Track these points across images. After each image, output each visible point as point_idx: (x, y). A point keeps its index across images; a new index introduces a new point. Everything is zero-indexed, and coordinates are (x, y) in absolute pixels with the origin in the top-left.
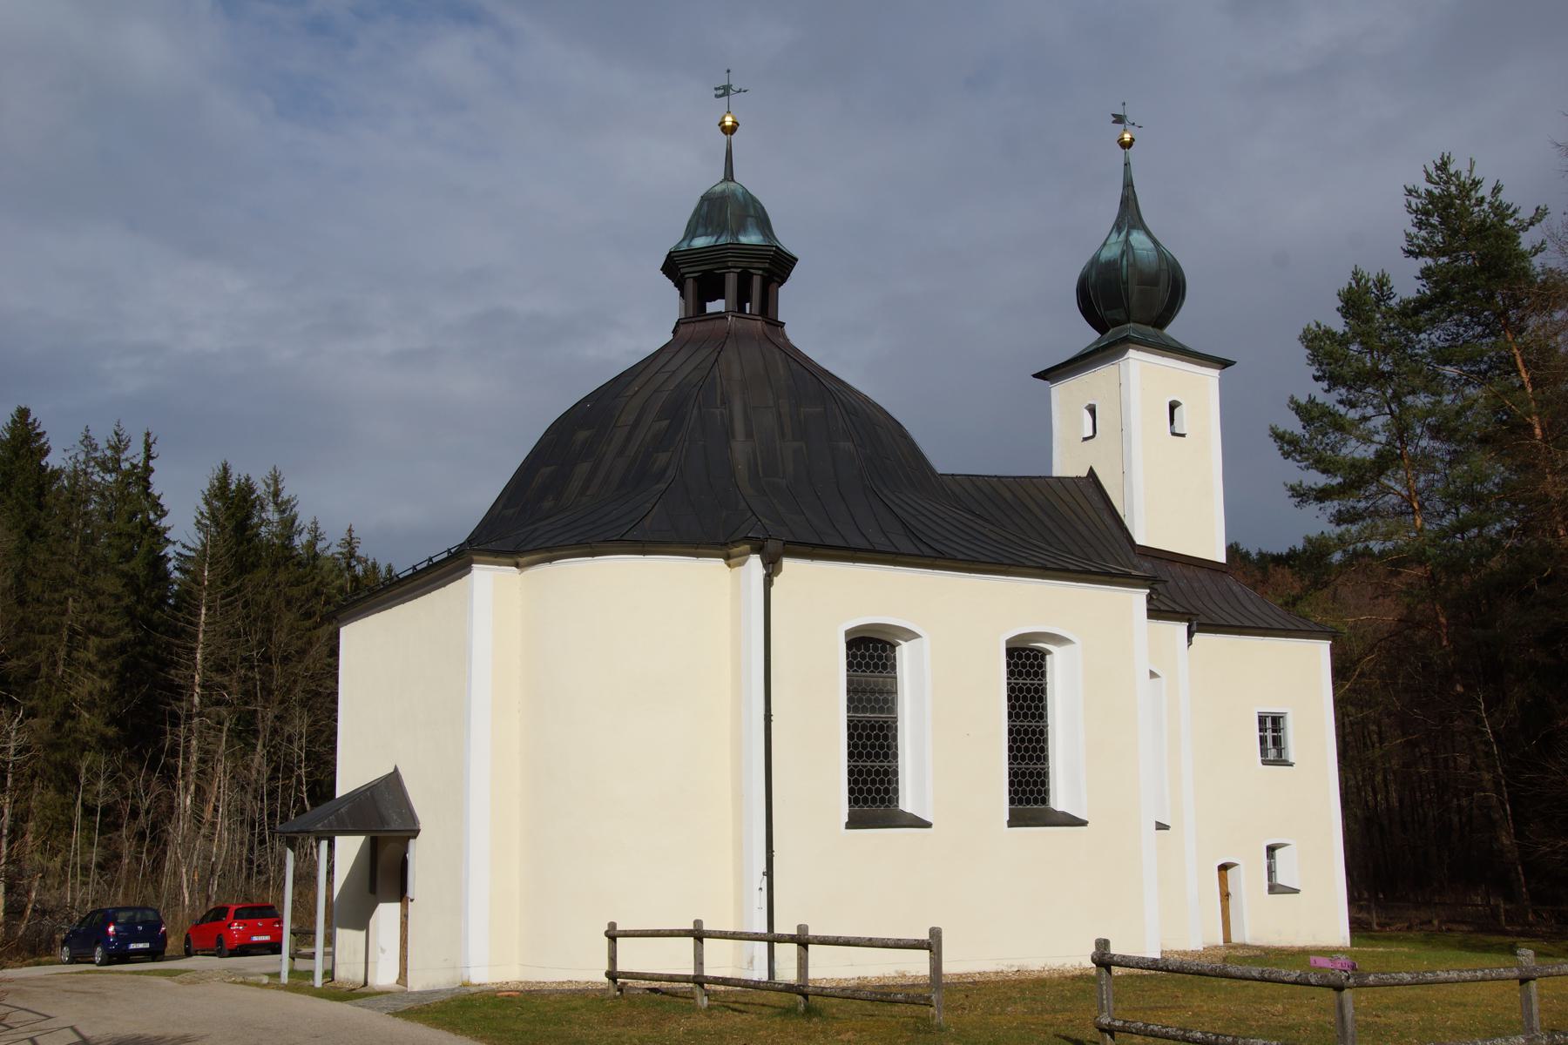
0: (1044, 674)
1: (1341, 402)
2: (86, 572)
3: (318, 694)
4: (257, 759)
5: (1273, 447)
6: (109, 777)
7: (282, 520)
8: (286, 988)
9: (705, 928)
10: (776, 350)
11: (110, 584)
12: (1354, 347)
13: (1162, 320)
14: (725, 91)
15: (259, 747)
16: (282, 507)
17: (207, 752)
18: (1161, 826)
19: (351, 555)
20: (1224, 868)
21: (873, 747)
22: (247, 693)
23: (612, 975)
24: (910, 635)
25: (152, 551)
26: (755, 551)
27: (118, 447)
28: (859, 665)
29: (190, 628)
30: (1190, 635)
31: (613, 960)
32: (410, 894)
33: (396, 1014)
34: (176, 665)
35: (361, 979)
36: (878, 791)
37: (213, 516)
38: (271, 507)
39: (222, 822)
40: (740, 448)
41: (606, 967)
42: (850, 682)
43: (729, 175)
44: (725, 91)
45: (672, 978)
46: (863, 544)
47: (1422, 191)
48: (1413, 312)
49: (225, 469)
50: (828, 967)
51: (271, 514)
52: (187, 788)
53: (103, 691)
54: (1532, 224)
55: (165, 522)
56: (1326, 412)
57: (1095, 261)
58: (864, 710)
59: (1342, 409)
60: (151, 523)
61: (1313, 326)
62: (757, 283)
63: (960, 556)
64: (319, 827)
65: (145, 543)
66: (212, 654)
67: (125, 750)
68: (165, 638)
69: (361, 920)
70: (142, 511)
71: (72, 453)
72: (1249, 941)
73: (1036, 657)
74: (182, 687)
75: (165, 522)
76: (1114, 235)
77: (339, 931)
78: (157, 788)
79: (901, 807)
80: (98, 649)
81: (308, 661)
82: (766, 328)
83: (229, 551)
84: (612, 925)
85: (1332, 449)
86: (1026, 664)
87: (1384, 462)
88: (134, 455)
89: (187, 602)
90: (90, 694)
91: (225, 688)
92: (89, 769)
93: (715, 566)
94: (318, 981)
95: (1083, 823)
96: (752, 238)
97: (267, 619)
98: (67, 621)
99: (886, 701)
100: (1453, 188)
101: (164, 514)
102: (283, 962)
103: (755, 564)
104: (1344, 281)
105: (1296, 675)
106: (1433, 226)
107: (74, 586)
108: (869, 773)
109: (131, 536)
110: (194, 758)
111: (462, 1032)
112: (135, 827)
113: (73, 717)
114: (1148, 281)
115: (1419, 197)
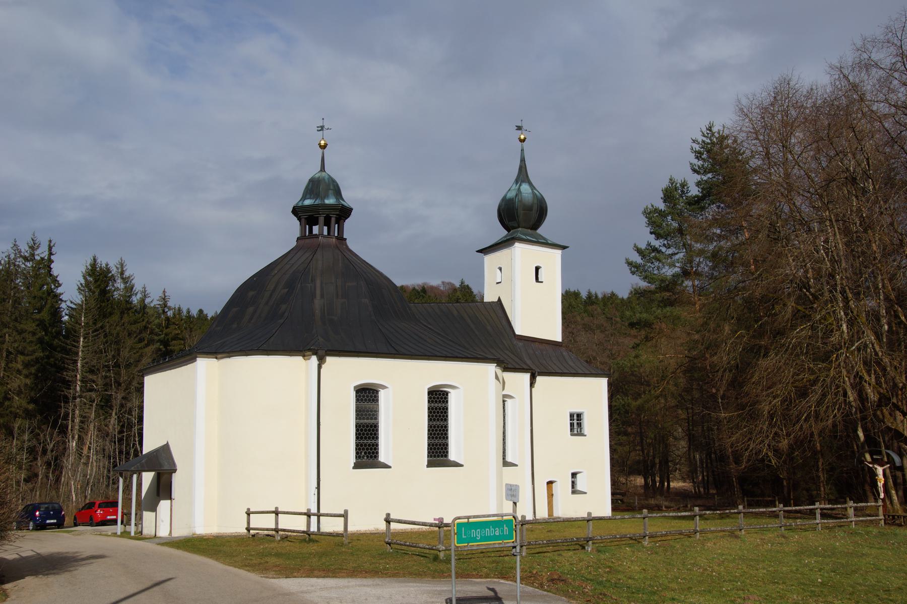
1: (664, 245)
2: (16, 320)
4: (113, 420)
6: (32, 432)
8: (119, 536)
11: (30, 326)
12: (669, 218)
13: (536, 225)
15: (114, 414)
16: (126, 280)
17: (85, 417)
19: (165, 306)
20: (550, 483)
23: (248, 529)
24: (384, 387)
25: (52, 306)
26: (314, 354)
31: (249, 523)
34: (67, 369)
38: (119, 281)
39: (93, 458)
40: (318, 303)
42: (357, 408)
44: (322, 128)
47: (700, 140)
48: (697, 203)
49: (95, 260)
51: (120, 284)
52: (73, 438)
53: (26, 385)
55: (60, 290)
56: (655, 250)
57: (505, 196)
58: (364, 419)
59: (663, 249)
61: (650, 206)
62: (333, 220)
64: (133, 468)
66: (86, 363)
67: (39, 417)
69: (153, 508)
70: (47, 284)
71: (6, 254)
75: (60, 290)
77: (145, 513)
78: (57, 438)
84: (249, 509)
86: (438, 400)
89: (72, 334)
90: (19, 386)
91: (94, 382)
92: (19, 428)
93: (299, 359)
96: (330, 201)
97: (117, 343)
98: (5, 346)
101: (60, 285)
102: (119, 528)
103: (314, 360)
104: (665, 184)
107: (9, 328)
108: (365, 445)
110: (77, 420)
112: (45, 459)
113: (9, 399)
114: (528, 208)
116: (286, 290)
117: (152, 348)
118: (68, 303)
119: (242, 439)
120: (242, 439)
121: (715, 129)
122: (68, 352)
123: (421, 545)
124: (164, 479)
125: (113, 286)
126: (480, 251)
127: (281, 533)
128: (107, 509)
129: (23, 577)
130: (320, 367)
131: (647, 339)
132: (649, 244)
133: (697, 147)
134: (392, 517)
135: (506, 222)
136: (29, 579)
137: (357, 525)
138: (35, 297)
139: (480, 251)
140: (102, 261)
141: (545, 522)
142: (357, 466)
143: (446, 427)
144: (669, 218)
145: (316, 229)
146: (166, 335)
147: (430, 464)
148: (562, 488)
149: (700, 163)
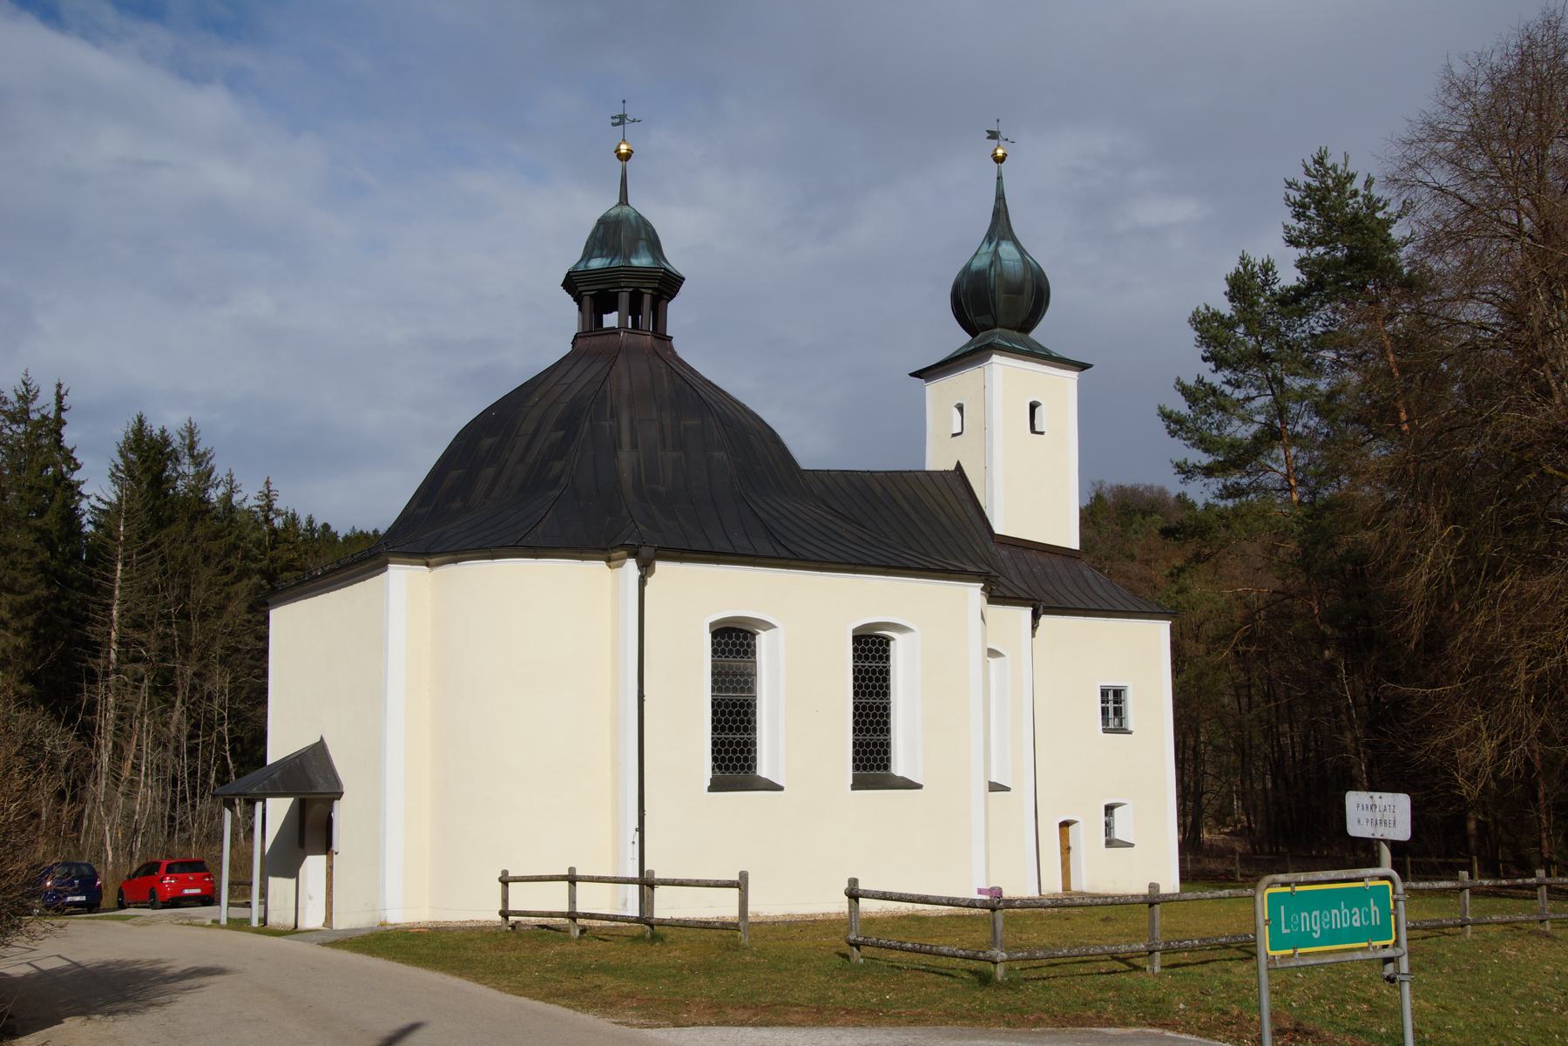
0: (888, 658)
1: (1229, 382)
3: (238, 650)
4: (176, 715)
5: (1161, 425)
7: (198, 475)
8: (222, 927)
9: (578, 873)
10: (662, 364)
12: (1241, 330)
14: (621, 120)
15: (178, 704)
16: (198, 460)
17: (125, 709)
18: (995, 787)
19: (269, 507)
20: (1065, 825)
21: (734, 721)
22: (164, 649)
23: (505, 914)
24: (768, 626)
25: (65, 505)
26: (631, 556)
27: (26, 398)
28: (723, 652)
29: (106, 584)
30: (1036, 617)
31: (505, 901)
32: (335, 847)
33: (324, 944)
35: (291, 922)
36: (738, 760)
37: (129, 470)
38: (187, 460)
40: (626, 458)
41: (500, 908)
42: (714, 667)
43: (624, 200)
44: (621, 120)
45: (551, 915)
46: (729, 549)
47: (1301, 184)
48: (1292, 301)
49: (141, 421)
50: (668, 904)
51: (187, 467)
53: (17, 648)
54: (1399, 216)
57: (966, 270)
58: (727, 690)
59: (1228, 389)
60: (63, 478)
61: (1202, 309)
62: (647, 300)
63: (813, 557)
65: (58, 497)
68: (79, 595)
70: (54, 465)
72: (1085, 889)
73: (881, 643)
74: (99, 644)
75: (76, 476)
76: (986, 246)
79: (759, 773)
80: (11, 605)
81: (226, 618)
82: (655, 342)
83: (145, 505)
84: (505, 873)
85: (1218, 428)
86: (871, 651)
87: (1271, 436)
88: (44, 404)
89: (100, 555)
91: (142, 644)
94: (255, 923)
95: (919, 787)
96: (642, 261)
97: (185, 574)
99: (746, 682)
100: (1330, 182)
101: (78, 467)
102: (223, 911)
103: (631, 566)
104: (1232, 266)
105: (1139, 653)
106: (1310, 218)
108: (731, 744)
109: (43, 490)
111: (378, 955)
114: (1015, 290)
115: (1299, 189)
116: (561, 433)
117: (243, 587)
118: (93, 501)
119: (482, 730)
120: (482, 730)
121: (1329, 163)
122: (93, 590)
123: (945, 950)
124: (314, 812)
125: (175, 470)
126: (917, 374)
127: (579, 921)
128: (182, 875)
129: (58, 1020)
130: (642, 583)
131: (1198, 558)
132: (1200, 381)
133: (1296, 195)
134: (862, 886)
135: (971, 317)
136: (72, 1024)
137: (768, 904)
138: (31, 488)
139: (917, 374)
140: (155, 426)
141: (1056, 903)
142: (716, 786)
143: (886, 708)
144: (1241, 330)
145: (611, 320)
146: (272, 561)
147: (858, 784)
148: (1088, 836)
149: (1302, 225)
